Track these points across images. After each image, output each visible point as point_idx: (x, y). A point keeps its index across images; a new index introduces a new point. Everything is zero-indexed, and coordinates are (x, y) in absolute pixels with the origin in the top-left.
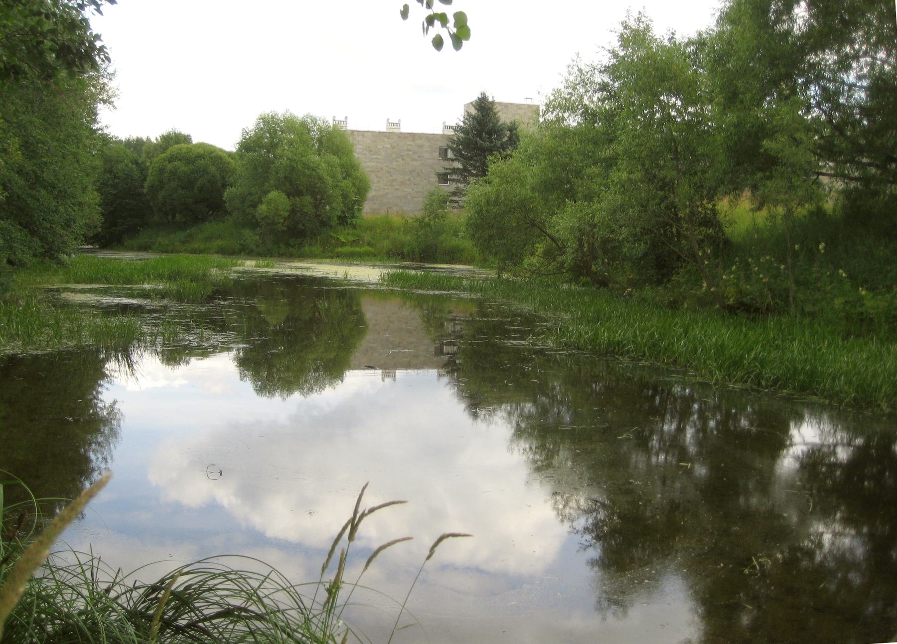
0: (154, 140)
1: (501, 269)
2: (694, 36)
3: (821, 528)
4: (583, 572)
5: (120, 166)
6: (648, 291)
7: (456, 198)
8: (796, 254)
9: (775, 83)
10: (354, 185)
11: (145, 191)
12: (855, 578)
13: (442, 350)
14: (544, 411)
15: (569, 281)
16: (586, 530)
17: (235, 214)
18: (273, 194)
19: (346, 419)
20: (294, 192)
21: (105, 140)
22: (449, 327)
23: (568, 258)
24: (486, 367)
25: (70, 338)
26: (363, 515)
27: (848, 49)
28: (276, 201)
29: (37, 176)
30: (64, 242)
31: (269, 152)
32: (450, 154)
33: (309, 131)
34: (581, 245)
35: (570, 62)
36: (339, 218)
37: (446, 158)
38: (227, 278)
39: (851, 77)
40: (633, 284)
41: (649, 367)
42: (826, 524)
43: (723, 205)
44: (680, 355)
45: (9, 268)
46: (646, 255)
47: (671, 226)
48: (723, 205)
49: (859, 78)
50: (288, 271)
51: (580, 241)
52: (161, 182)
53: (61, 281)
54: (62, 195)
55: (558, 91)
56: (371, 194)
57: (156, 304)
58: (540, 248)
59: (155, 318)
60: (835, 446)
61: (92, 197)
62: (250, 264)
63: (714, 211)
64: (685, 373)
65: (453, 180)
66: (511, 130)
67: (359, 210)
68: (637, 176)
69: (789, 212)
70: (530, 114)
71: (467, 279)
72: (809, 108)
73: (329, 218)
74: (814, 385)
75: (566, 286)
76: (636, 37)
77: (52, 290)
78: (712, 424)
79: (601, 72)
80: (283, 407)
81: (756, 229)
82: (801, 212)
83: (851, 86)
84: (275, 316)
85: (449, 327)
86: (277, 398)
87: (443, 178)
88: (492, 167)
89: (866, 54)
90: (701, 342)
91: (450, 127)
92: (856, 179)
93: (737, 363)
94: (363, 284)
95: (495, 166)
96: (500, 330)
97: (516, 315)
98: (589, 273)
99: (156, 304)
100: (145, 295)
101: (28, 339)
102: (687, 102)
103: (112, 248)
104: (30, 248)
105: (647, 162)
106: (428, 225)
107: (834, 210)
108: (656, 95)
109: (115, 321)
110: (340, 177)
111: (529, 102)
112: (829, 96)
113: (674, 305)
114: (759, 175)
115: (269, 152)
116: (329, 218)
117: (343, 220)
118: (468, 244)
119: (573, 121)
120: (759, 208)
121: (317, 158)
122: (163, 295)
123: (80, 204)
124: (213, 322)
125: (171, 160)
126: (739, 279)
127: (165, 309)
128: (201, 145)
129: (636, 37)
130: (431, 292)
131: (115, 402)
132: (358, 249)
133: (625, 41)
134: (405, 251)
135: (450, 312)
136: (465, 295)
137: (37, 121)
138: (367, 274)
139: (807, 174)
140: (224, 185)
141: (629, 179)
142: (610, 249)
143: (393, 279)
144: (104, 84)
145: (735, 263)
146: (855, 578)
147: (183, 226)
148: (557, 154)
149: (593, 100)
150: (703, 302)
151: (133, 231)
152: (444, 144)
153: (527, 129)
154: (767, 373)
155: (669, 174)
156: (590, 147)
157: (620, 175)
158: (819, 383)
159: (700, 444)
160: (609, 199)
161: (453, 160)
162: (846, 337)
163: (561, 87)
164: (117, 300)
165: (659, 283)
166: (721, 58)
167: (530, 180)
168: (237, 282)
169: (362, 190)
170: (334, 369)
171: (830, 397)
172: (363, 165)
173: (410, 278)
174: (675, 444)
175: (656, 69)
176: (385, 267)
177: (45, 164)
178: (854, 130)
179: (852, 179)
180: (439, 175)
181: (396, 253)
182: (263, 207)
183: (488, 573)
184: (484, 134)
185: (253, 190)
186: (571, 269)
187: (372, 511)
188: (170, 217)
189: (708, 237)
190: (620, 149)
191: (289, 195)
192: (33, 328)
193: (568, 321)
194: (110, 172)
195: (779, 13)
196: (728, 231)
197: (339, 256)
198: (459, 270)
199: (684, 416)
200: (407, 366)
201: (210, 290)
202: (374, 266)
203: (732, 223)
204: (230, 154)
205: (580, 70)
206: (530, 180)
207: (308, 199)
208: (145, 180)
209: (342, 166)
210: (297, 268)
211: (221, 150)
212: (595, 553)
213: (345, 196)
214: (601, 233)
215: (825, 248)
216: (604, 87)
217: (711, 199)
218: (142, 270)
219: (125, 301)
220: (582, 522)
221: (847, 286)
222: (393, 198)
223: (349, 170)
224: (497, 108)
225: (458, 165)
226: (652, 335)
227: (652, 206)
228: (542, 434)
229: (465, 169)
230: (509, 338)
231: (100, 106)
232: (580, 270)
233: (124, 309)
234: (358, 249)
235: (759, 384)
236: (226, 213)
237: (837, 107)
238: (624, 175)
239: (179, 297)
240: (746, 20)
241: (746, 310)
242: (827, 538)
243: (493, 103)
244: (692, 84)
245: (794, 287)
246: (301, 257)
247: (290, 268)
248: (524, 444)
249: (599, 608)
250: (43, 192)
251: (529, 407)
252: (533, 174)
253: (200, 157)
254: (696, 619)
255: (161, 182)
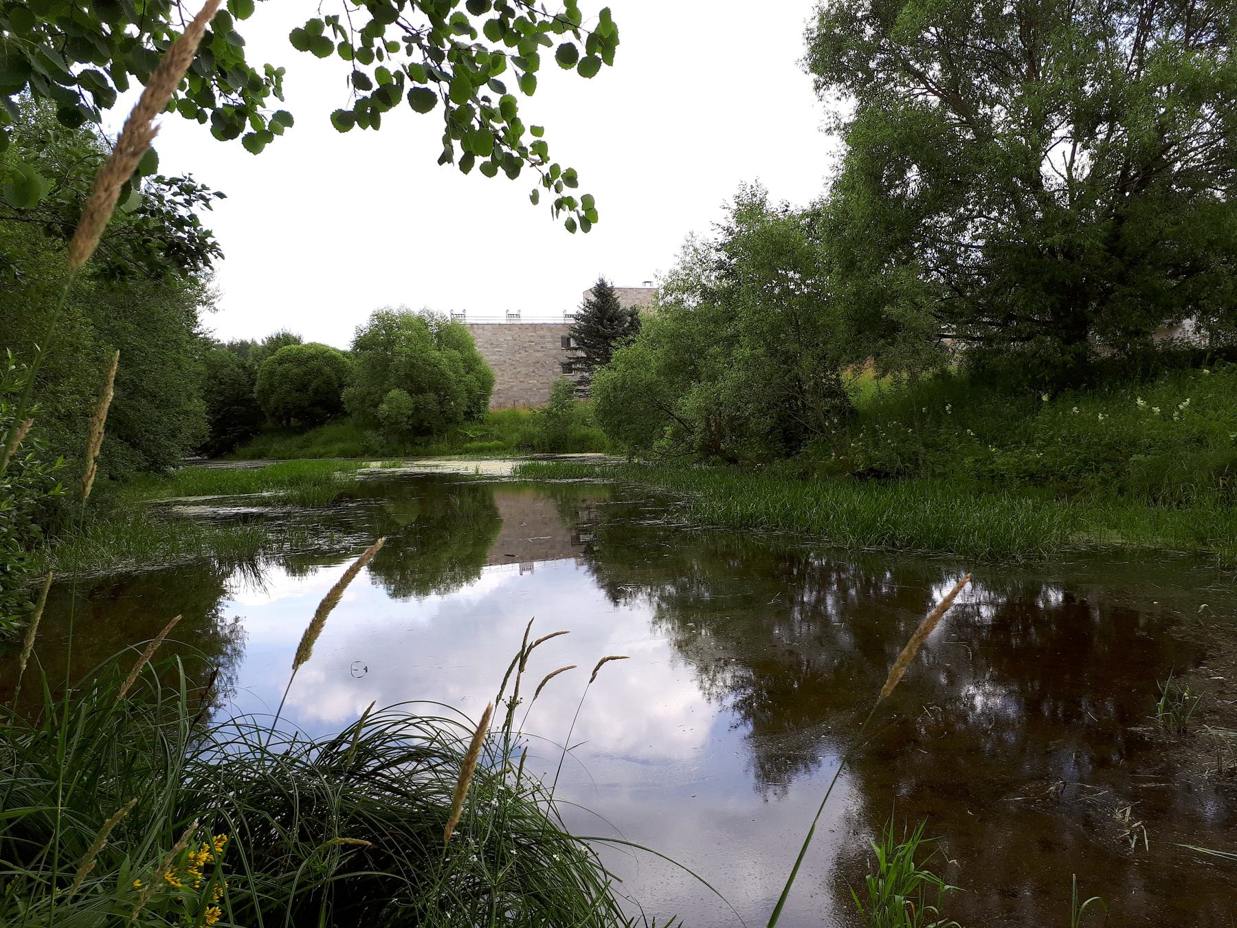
0: (260, 343)
1: (632, 455)
2: (807, 207)
3: (972, 690)
4: (739, 752)
5: (226, 371)
6: (777, 465)
7: (582, 387)
8: (923, 417)
9: (892, 249)
10: (478, 379)
11: (255, 396)
12: (1010, 738)
13: (578, 538)
14: (683, 589)
15: (699, 461)
16: (736, 707)
17: (355, 414)
18: (394, 393)
19: (491, 609)
20: (416, 390)
21: (207, 344)
22: (584, 515)
23: (697, 438)
24: (622, 552)
25: (189, 551)
26: (531, 647)
27: (962, 210)
28: (397, 399)
29: (135, 386)
30: (170, 454)
31: (386, 349)
32: (573, 344)
33: (426, 326)
34: (708, 425)
35: (685, 243)
36: (466, 413)
37: (569, 348)
38: (352, 481)
39: (966, 238)
40: (760, 458)
41: (784, 537)
42: (977, 686)
43: (846, 375)
44: (813, 522)
45: (113, 485)
46: (773, 429)
47: (796, 399)
48: (846, 375)
49: (975, 238)
50: (417, 470)
51: (708, 420)
52: (271, 385)
53: (171, 495)
54: (164, 404)
55: (676, 273)
56: (495, 388)
57: (279, 511)
58: (669, 430)
59: (280, 525)
60: (978, 604)
61: (198, 405)
62: (375, 466)
63: (838, 381)
64: (819, 540)
65: (578, 369)
66: (631, 316)
67: (486, 405)
68: (761, 351)
69: (914, 377)
70: (649, 298)
71: (599, 466)
72: (928, 271)
73: (455, 414)
74: (949, 543)
75: (696, 466)
76: (750, 211)
77: (161, 505)
78: (853, 592)
79: (717, 250)
80: (422, 609)
81: (881, 395)
82: (926, 375)
83: (967, 246)
84: (405, 515)
85: (584, 515)
86: (413, 599)
87: (568, 368)
88: (615, 354)
89: (980, 215)
90: (833, 509)
91: (571, 316)
92: (979, 339)
93: (869, 527)
94: (496, 478)
95: (619, 352)
96: (635, 512)
97: (649, 497)
98: (718, 451)
99: (279, 511)
100: (265, 503)
101: (143, 557)
102: (806, 274)
103: (222, 458)
104: (132, 462)
105: (768, 337)
106: (557, 415)
107: (959, 371)
108: (774, 269)
109: (237, 531)
110: (463, 372)
111: (648, 285)
112: (947, 259)
113: (804, 476)
114: (882, 341)
115: (386, 349)
116: (455, 414)
117: (469, 415)
118: (597, 432)
119: (692, 302)
120: (883, 376)
121: (437, 353)
122: (285, 502)
123: (186, 413)
124: (342, 524)
125: (281, 362)
126: (867, 446)
127: (288, 515)
128: (312, 345)
129: (750, 211)
130: (564, 481)
131: (237, 619)
132: (487, 444)
133: (739, 217)
134: (535, 442)
135: (584, 501)
136: (597, 481)
137: (131, 327)
138: (499, 467)
139: (929, 338)
140: (341, 386)
141: (752, 355)
142: (738, 427)
143: (524, 470)
144: (203, 285)
145: (862, 431)
146: (1010, 738)
147: (300, 431)
148: (679, 336)
149: (711, 280)
150: (831, 472)
151: (244, 439)
152: (566, 334)
153: (649, 312)
154: (901, 534)
155: (793, 347)
156: (711, 327)
157: (742, 352)
158: (953, 540)
159: (842, 613)
160: (736, 375)
161: (576, 349)
162: (978, 496)
163: (678, 268)
164: (235, 510)
165: (788, 455)
166: (836, 227)
167: (654, 364)
168: (363, 484)
169: (486, 383)
170: (469, 567)
171: (965, 553)
172: (485, 358)
173: (543, 468)
174: (816, 613)
175: (774, 243)
176: (515, 460)
177: (144, 372)
178: (974, 290)
179: (974, 339)
180: (563, 365)
181: (525, 446)
182: (384, 407)
183: (636, 761)
184: (604, 320)
185: (373, 389)
186: (701, 449)
187: (538, 643)
188: (284, 422)
189: (834, 407)
190: (741, 326)
191: (410, 392)
192: (146, 544)
193: (703, 497)
194: (215, 378)
195: (891, 179)
196: (853, 400)
197: (467, 451)
198: (590, 458)
199: (822, 583)
200: (545, 557)
201: (335, 493)
202: (504, 459)
203: (857, 390)
204: (344, 354)
205: (695, 250)
206: (654, 364)
207: (431, 396)
208: (253, 384)
209: (464, 361)
210: (425, 466)
211: (334, 349)
212: (748, 729)
213: (470, 391)
214: (727, 412)
215: (951, 409)
216: (721, 265)
217: (834, 370)
218: (259, 478)
219: (244, 510)
220: (731, 700)
221: (977, 444)
222: (519, 389)
223: (472, 364)
224: (617, 294)
225: (581, 354)
226: (784, 505)
227: (776, 380)
228: (682, 612)
229: (589, 358)
230: (645, 519)
231: (199, 308)
232: (709, 449)
233: (245, 518)
234: (487, 444)
235: (894, 544)
236: (345, 414)
237: (955, 268)
238: (748, 352)
239: (303, 503)
240: (860, 186)
241: (877, 475)
242: (979, 701)
243: (612, 289)
244: (810, 256)
245: (923, 451)
246: (429, 455)
247: (419, 466)
248: (666, 625)
249: (757, 789)
250: (144, 401)
251: (670, 589)
252: (656, 358)
253: (313, 357)
254: (855, 791)
255: (271, 385)
